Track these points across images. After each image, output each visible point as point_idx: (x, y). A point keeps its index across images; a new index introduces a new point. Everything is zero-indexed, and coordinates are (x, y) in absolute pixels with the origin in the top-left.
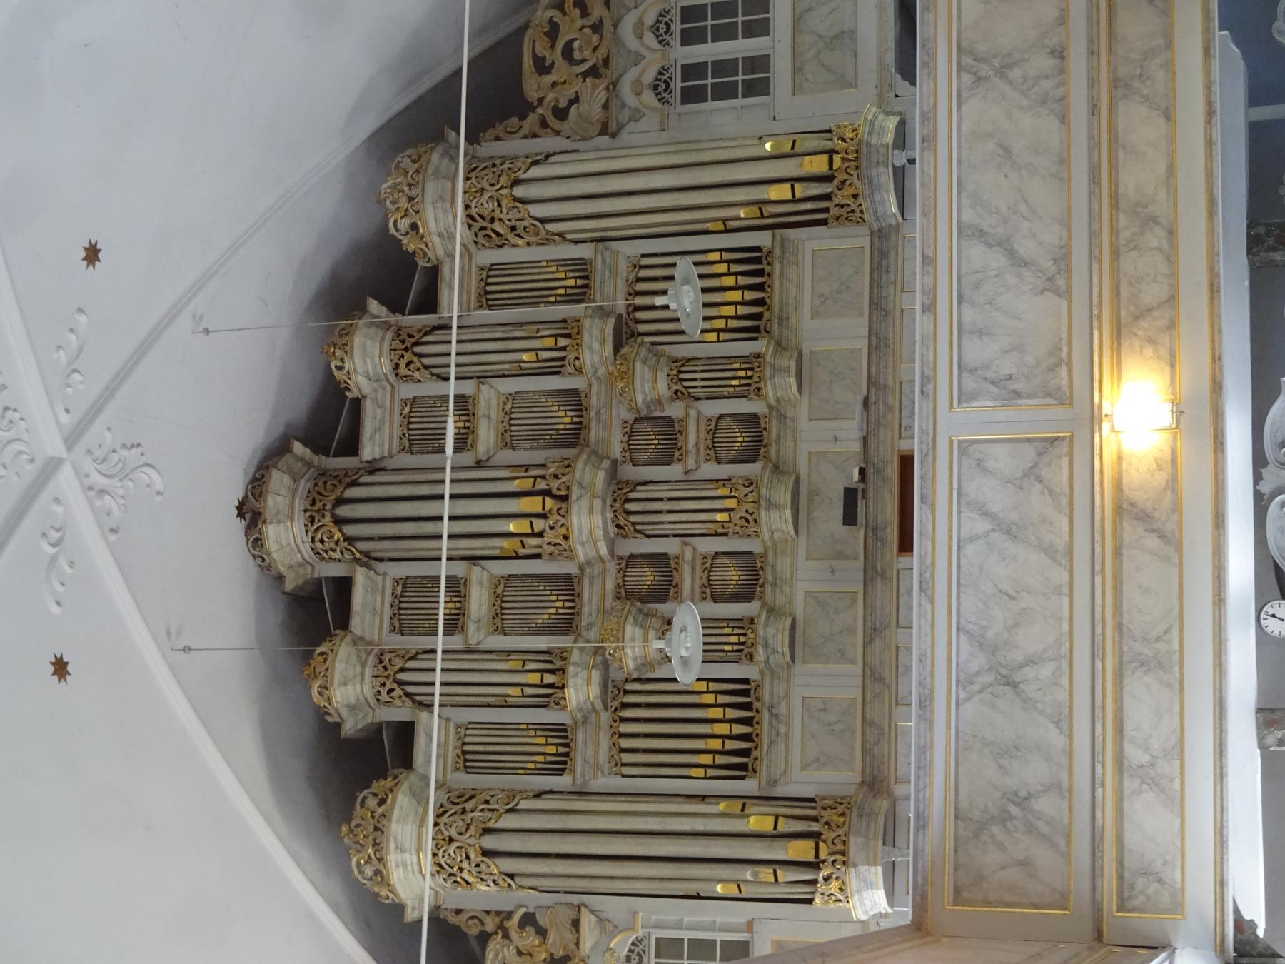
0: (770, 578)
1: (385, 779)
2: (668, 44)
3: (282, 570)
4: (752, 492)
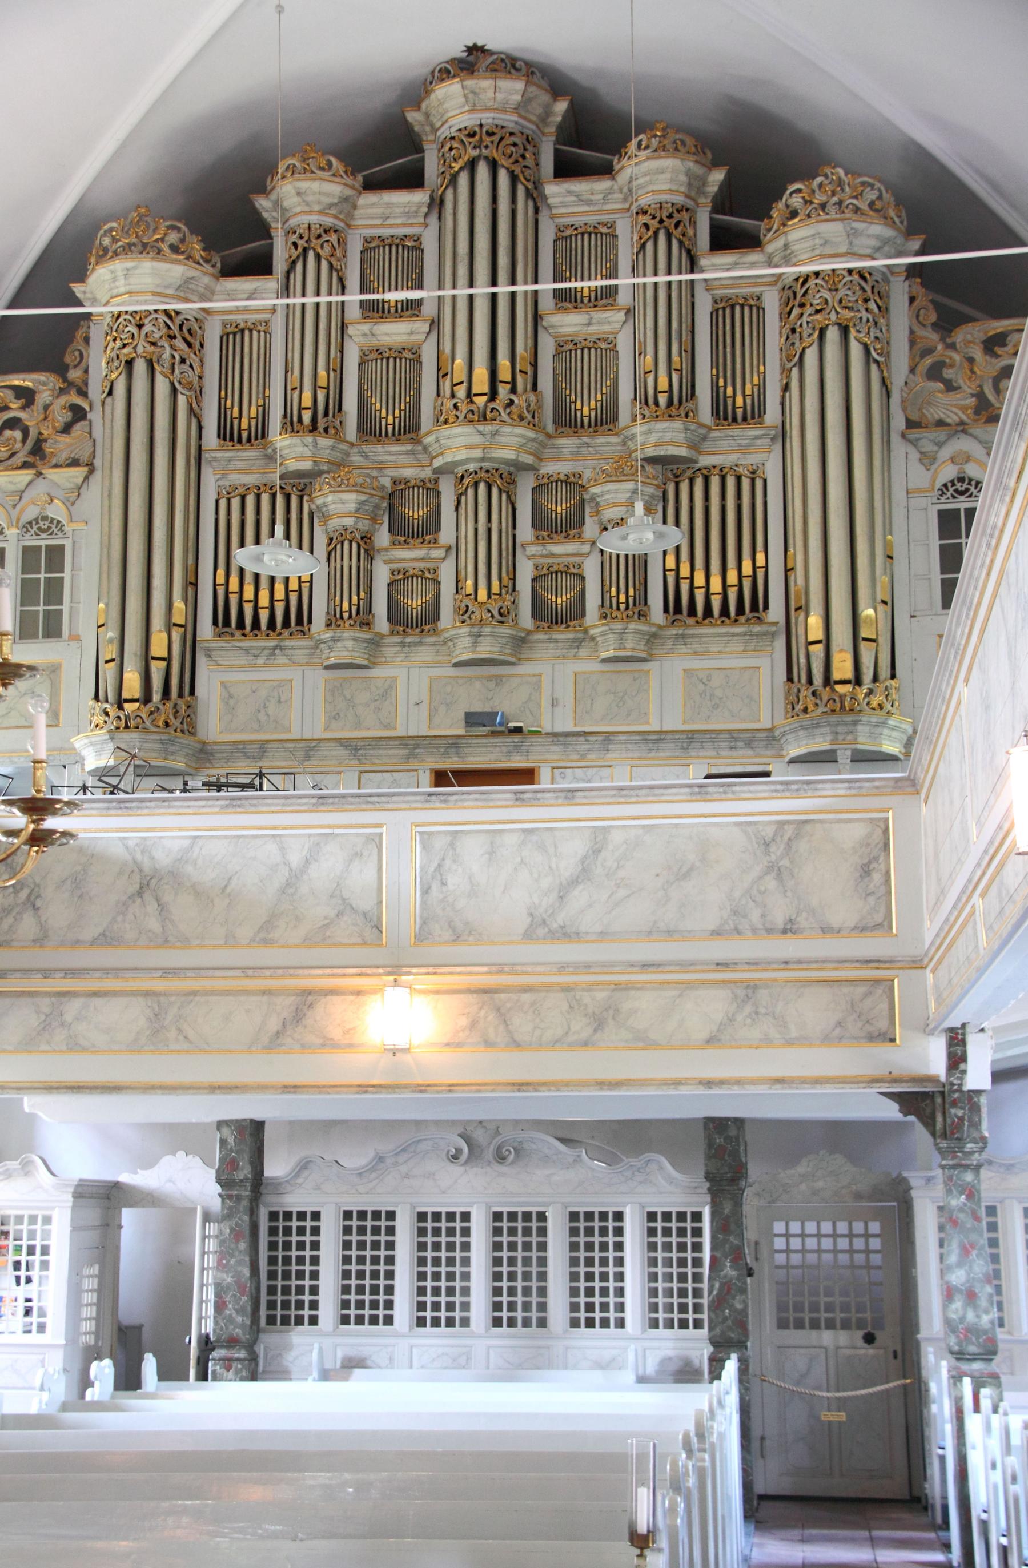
0: (408, 640)
1: (204, 250)
2: (943, 494)
3: (424, 106)
4: (492, 616)
